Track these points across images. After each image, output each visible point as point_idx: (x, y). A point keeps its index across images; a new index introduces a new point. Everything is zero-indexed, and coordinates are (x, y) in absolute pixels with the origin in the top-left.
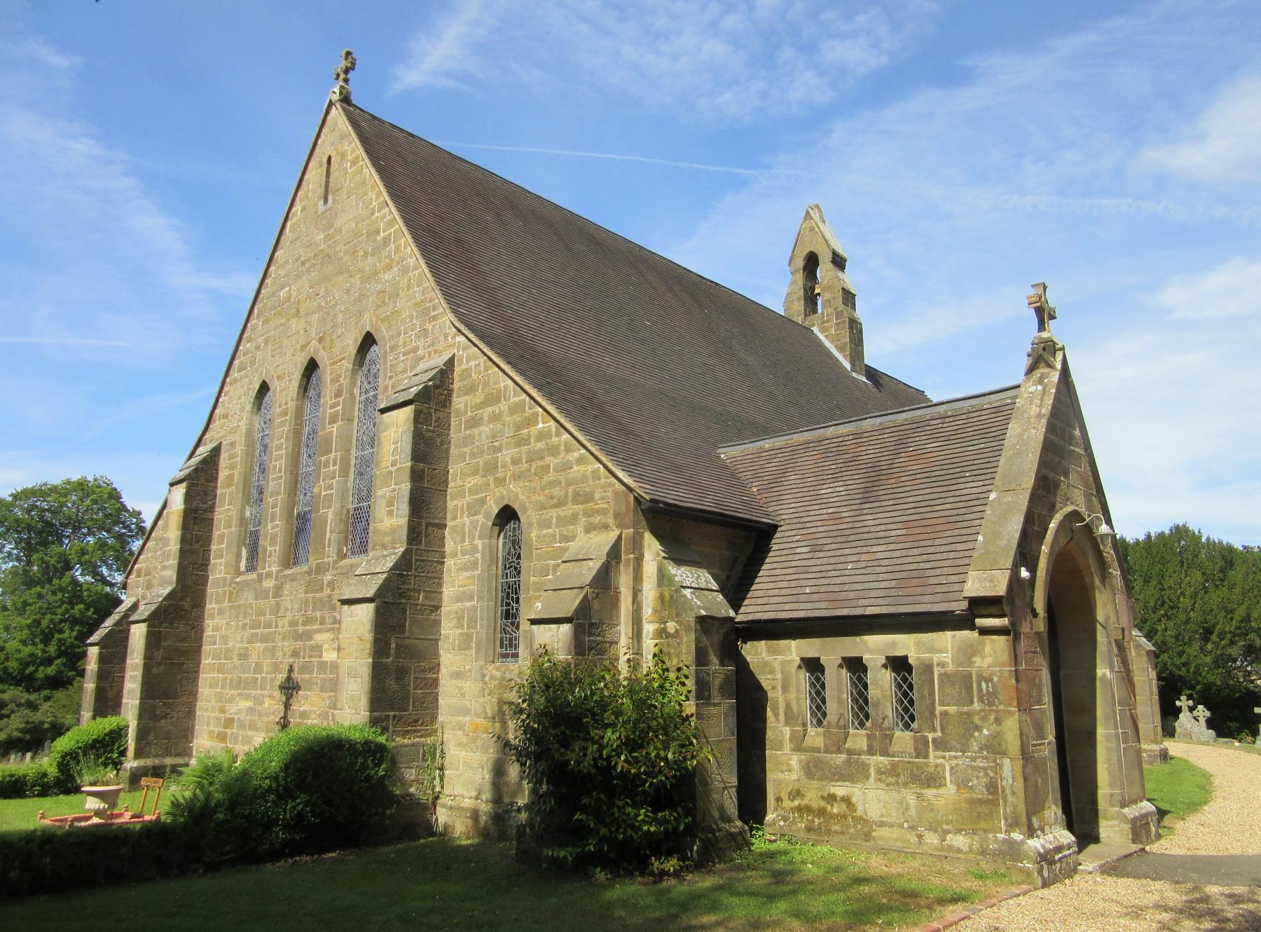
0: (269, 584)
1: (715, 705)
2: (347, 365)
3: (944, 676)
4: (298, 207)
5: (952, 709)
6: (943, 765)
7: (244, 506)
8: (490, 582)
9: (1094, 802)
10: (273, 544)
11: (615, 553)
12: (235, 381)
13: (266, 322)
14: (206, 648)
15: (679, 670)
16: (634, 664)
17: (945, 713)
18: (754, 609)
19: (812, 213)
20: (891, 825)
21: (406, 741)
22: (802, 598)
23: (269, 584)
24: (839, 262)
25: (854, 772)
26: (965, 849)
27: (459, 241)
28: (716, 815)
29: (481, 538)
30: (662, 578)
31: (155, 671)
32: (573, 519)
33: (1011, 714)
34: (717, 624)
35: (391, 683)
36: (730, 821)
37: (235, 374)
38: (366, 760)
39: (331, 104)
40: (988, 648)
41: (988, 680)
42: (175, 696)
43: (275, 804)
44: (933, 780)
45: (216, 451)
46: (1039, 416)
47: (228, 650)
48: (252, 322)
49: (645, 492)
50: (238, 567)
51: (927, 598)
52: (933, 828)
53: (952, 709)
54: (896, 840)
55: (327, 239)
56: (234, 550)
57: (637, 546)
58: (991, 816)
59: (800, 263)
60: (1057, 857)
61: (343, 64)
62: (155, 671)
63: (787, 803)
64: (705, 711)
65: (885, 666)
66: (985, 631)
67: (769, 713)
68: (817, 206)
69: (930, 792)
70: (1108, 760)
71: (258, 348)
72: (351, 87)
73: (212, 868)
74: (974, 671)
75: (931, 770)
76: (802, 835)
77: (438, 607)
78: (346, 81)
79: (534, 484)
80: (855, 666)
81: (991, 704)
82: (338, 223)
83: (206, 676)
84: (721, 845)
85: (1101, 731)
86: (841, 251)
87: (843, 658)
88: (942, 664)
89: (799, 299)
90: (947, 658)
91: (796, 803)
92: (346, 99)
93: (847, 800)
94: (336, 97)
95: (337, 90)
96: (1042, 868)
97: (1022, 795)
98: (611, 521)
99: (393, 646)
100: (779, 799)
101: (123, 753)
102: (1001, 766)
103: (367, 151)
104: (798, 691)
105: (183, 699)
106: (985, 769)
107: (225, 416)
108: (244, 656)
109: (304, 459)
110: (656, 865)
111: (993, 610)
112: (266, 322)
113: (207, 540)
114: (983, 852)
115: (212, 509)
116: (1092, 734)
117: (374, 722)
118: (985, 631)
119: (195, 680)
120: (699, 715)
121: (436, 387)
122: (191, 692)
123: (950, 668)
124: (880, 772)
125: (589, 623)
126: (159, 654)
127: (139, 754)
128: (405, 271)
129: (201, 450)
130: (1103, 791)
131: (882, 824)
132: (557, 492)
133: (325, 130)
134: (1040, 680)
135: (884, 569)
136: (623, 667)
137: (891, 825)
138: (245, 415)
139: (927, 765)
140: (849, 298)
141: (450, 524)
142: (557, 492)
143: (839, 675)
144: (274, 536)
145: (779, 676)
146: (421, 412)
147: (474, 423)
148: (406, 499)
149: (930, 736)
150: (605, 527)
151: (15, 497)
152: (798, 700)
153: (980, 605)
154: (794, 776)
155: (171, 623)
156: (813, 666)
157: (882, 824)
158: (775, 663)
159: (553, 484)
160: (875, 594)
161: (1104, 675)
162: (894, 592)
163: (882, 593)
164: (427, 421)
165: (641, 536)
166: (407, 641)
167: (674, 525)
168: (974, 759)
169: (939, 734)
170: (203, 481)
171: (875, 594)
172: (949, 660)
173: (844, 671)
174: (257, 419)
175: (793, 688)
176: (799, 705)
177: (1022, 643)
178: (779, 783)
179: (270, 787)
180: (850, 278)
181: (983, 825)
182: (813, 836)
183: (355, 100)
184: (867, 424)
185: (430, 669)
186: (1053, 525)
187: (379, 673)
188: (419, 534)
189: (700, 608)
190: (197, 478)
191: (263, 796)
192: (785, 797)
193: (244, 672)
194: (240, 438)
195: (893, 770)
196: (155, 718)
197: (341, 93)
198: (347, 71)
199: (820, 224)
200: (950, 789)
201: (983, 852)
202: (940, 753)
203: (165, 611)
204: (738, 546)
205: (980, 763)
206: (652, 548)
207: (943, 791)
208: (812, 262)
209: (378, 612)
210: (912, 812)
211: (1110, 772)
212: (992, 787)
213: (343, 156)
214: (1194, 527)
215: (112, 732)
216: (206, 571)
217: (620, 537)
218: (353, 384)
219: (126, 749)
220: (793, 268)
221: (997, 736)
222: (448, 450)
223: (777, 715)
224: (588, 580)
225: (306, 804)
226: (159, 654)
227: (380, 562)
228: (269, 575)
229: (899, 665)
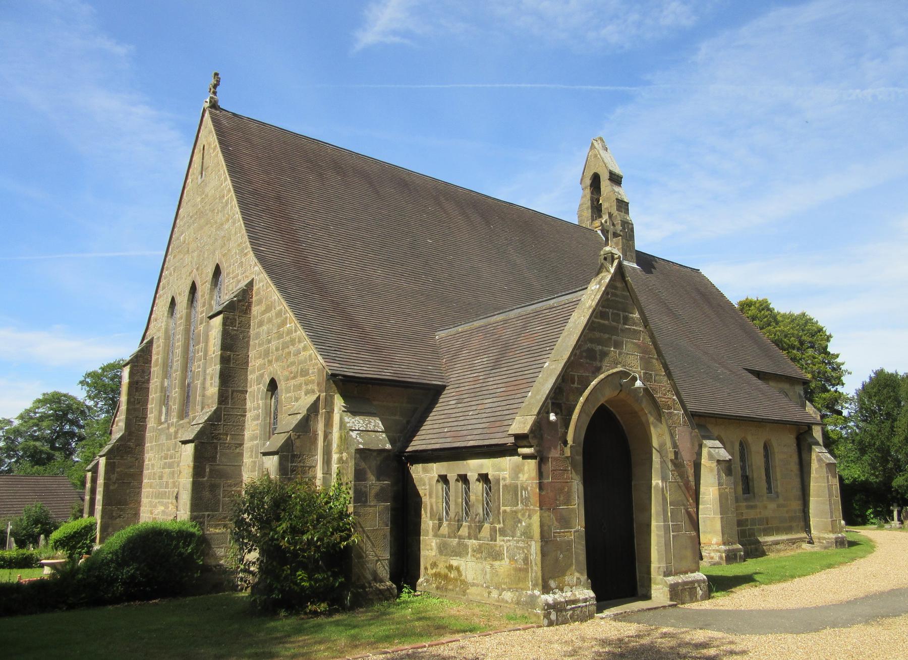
0: (172, 430)
1: (371, 506)
2: (208, 285)
3: (505, 486)
4: (189, 180)
5: (508, 509)
6: (502, 546)
7: (163, 379)
8: (265, 428)
9: (649, 573)
10: (174, 404)
11: (314, 409)
12: (161, 296)
13: (174, 257)
14: (145, 472)
15: (347, 484)
16: (326, 481)
17: (505, 511)
18: (417, 444)
19: (595, 144)
20: (477, 585)
21: (217, 531)
22: (442, 435)
23: (172, 430)
24: (616, 179)
25: (460, 552)
26: (510, 601)
27: (279, 198)
28: (370, 577)
29: (262, 399)
30: (342, 424)
31: (111, 488)
32: (298, 387)
33: (536, 512)
34: (375, 454)
35: (207, 494)
36: (381, 581)
37: (160, 292)
38: (178, 544)
39: (204, 111)
40: (526, 468)
41: (526, 489)
42: (126, 503)
43: (117, 569)
44: (496, 556)
45: (151, 342)
46: (590, 307)
47: (154, 474)
48: (169, 257)
49: (337, 368)
50: (160, 419)
51: (500, 435)
52: (497, 588)
53: (508, 509)
54: (478, 595)
55: (202, 201)
56: (158, 408)
57: (329, 403)
58: (525, 579)
59: (588, 182)
60: (569, 607)
61: (213, 81)
62: (111, 488)
63: (430, 571)
64: (362, 510)
65: (478, 480)
66: (525, 457)
67: (423, 512)
68: (601, 139)
69: (497, 563)
70: (658, 543)
71: (170, 274)
72: (218, 97)
73: (71, 607)
74: (519, 483)
75: (498, 549)
76: (434, 592)
77: (241, 445)
78: (215, 93)
79: (284, 364)
80: (463, 479)
81: (526, 505)
82: (207, 190)
83: (146, 491)
84: (370, 597)
85: (654, 524)
86: (617, 170)
87: (459, 475)
88: (504, 479)
89: (587, 209)
90: (506, 474)
91: (434, 571)
92: (214, 105)
93: (458, 569)
94: (208, 105)
95: (208, 100)
96: (550, 613)
97: (540, 565)
98: (316, 388)
99: (208, 470)
100: (426, 569)
101: (93, 540)
102: (530, 546)
103: (220, 142)
104: (437, 497)
105: (131, 506)
106: (523, 548)
107: (156, 320)
108: (161, 477)
109: (191, 348)
110: (310, 607)
111: (525, 443)
112: (174, 257)
113: (145, 402)
114: (518, 603)
115: (148, 381)
116: (649, 525)
117: (193, 518)
118: (525, 457)
119: (139, 493)
120: (355, 513)
121: (239, 301)
122: (136, 501)
123: (508, 481)
124: (474, 551)
125: (293, 454)
126: (114, 477)
127: (101, 541)
128: (234, 223)
129: (145, 341)
130: (654, 565)
131: (473, 585)
132: (294, 369)
133: (202, 128)
134: (570, 488)
135: (486, 415)
136: (319, 482)
137: (477, 585)
138: (165, 319)
139: (495, 545)
140: (623, 206)
141: (249, 390)
142: (294, 369)
143: (456, 486)
144: (175, 398)
145: (428, 487)
146: (228, 318)
147: (261, 324)
148: (218, 376)
149: (498, 526)
150: (313, 392)
151: (103, 369)
152: (437, 503)
153: (520, 439)
154: (434, 554)
155: (122, 457)
156: (444, 479)
157: (473, 585)
158: (425, 476)
159: (293, 363)
160: (476, 432)
161: (657, 484)
162: (485, 431)
163: (479, 431)
164: (233, 324)
165: (332, 397)
166: (218, 467)
167: (357, 391)
168: (518, 542)
169: (502, 525)
170: (141, 363)
171: (476, 432)
172: (507, 476)
173: (460, 484)
174: (171, 322)
175: (434, 496)
176: (437, 507)
177: (550, 466)
178: (426, 557)
179: (112, 559)
180: (624, 192)
181: (521, 585)
182: (439, 593)
183: (221, 104)
184: (512, 314)
185: (235, 485)
186: (594, 383)
187: (197, 487)
188: (227, 398)
189: (361, 443)
190: (137, 361)
191: (108, 564)
192: (429, 567)
193: (161, 487)
194: (161, 334)
195: (479, 550)
196: (112, 518)
197: (211, 101)
198: (215, 86)
199: (602, 152)
200: (506, 561)
201: (518, 603)
202: (502, 538)
203: (118, 448)
204: (411, 401)
205: (521, 544)
206: (339, 403)
207: (503, 562)
208: (596, 181)
209: (196, 448)
210: (488, 576)
211: (658, 552)
212: (526, 560)
213: (210, 144)
214: (889, 370)
215: (86, 527)
216: (145, 422)
217: (319, 396)
218: (211, 298)
219: (95, 538)
220: (584, 186)
221: (529, 526)
222: (248, 342)
223: (426, 513)
224: (292, 426)
225: (137, 569)
226: (114, 477)
227: (201, 416)
228: (172, 424)
229: (484, 478)
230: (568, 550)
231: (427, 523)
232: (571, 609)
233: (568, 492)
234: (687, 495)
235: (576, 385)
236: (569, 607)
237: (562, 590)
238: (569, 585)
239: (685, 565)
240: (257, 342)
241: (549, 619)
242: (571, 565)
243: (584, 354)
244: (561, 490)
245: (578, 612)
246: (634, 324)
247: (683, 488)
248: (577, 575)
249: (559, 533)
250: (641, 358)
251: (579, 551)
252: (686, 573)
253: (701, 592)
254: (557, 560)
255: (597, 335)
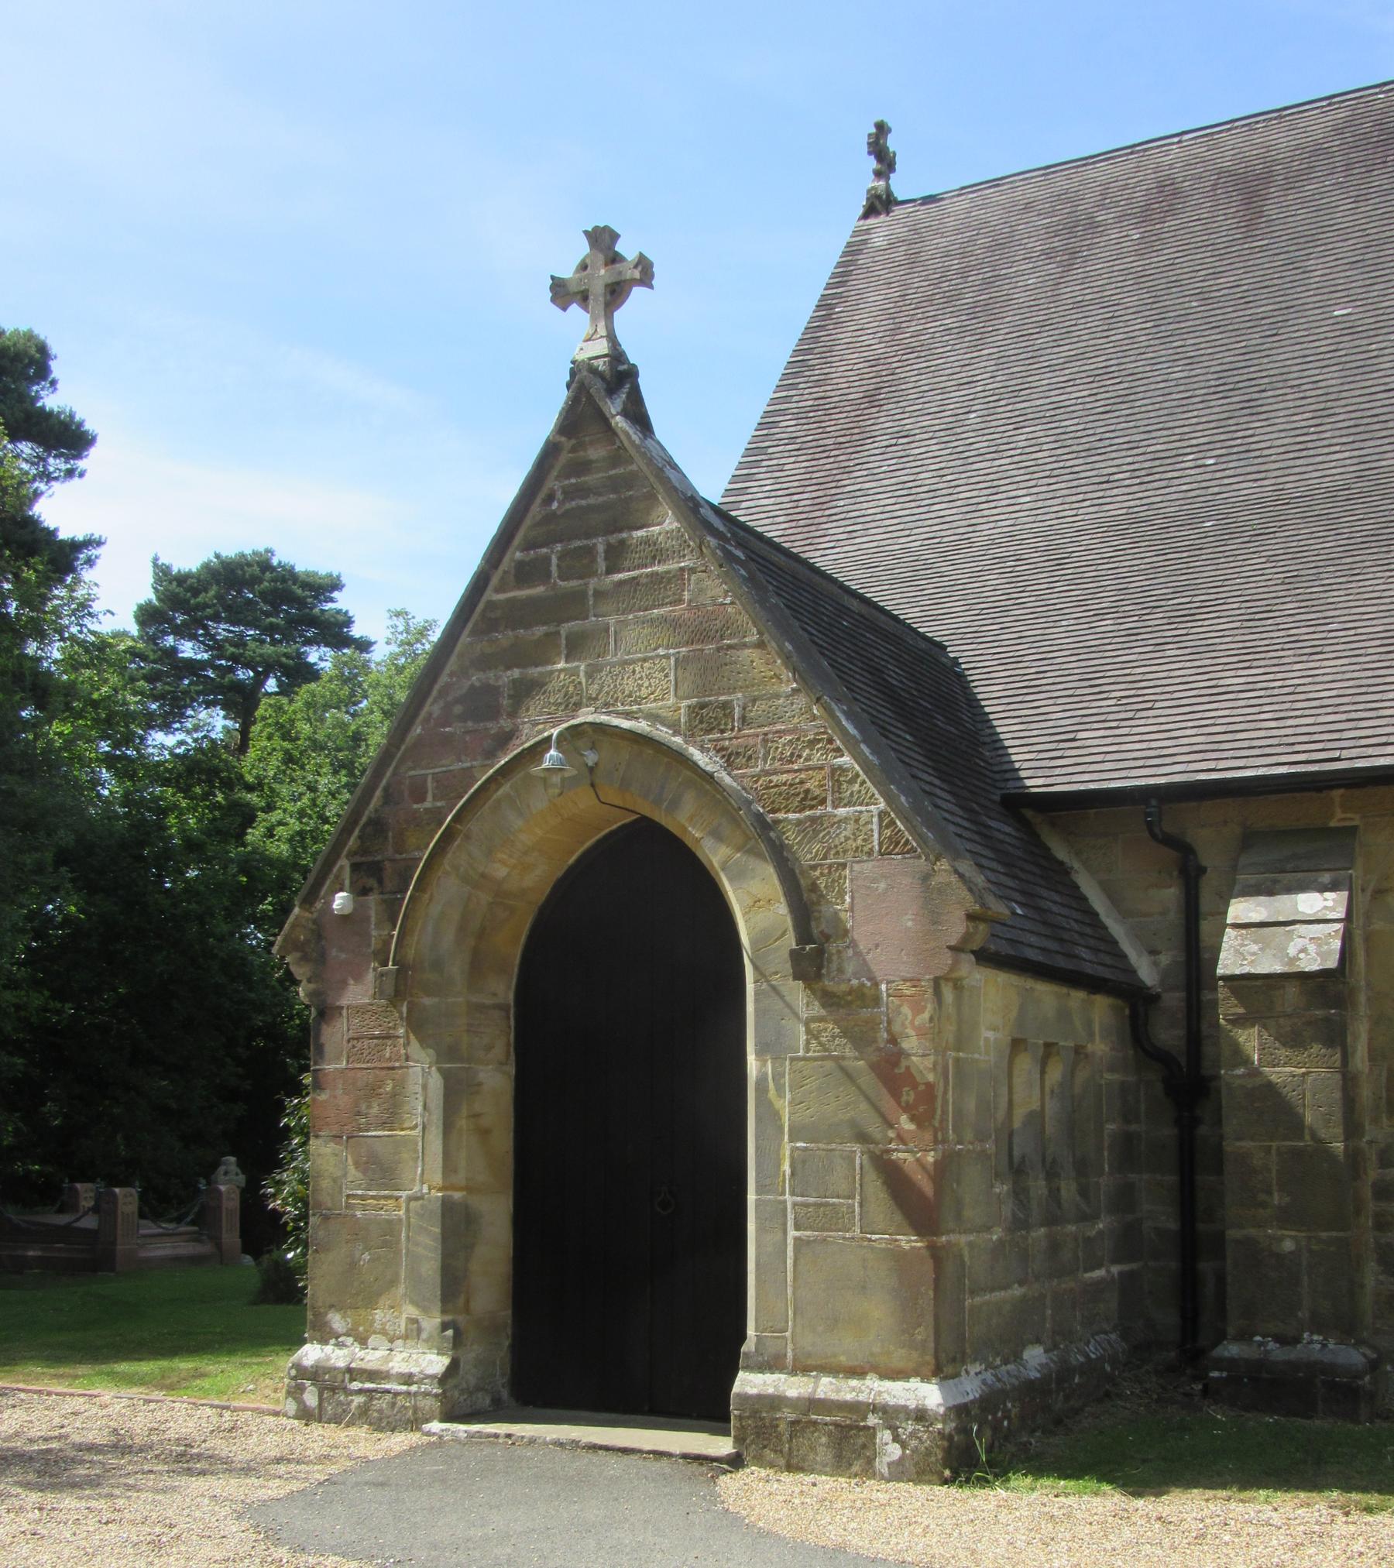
60: (356, 1385)
96: (301, 1389)
230: (385, 1244)
231: (1253, 971)
232: (360, 1391)
233: (394, 1095)
234: (887, 1103)
235: (428, 804)
236: (356, 1385)
237: (363, 1341)
238: (383, 1332)
239: (846, 1346)
240: (190, 741)
241: (300, 1402)
242: (393, 1282)
243: (458, 709)
244: (373, 1091)
245: (382, 1403)
246: (658, 554)
247: (868, 1080)
248: (411, 1311)
249: (362, 1198)
250: (681, 663)
251: (422, 1251)
252: (857, 1372)
253: (894, 1451)
254: (353, 1265)
255: (504, 638)
